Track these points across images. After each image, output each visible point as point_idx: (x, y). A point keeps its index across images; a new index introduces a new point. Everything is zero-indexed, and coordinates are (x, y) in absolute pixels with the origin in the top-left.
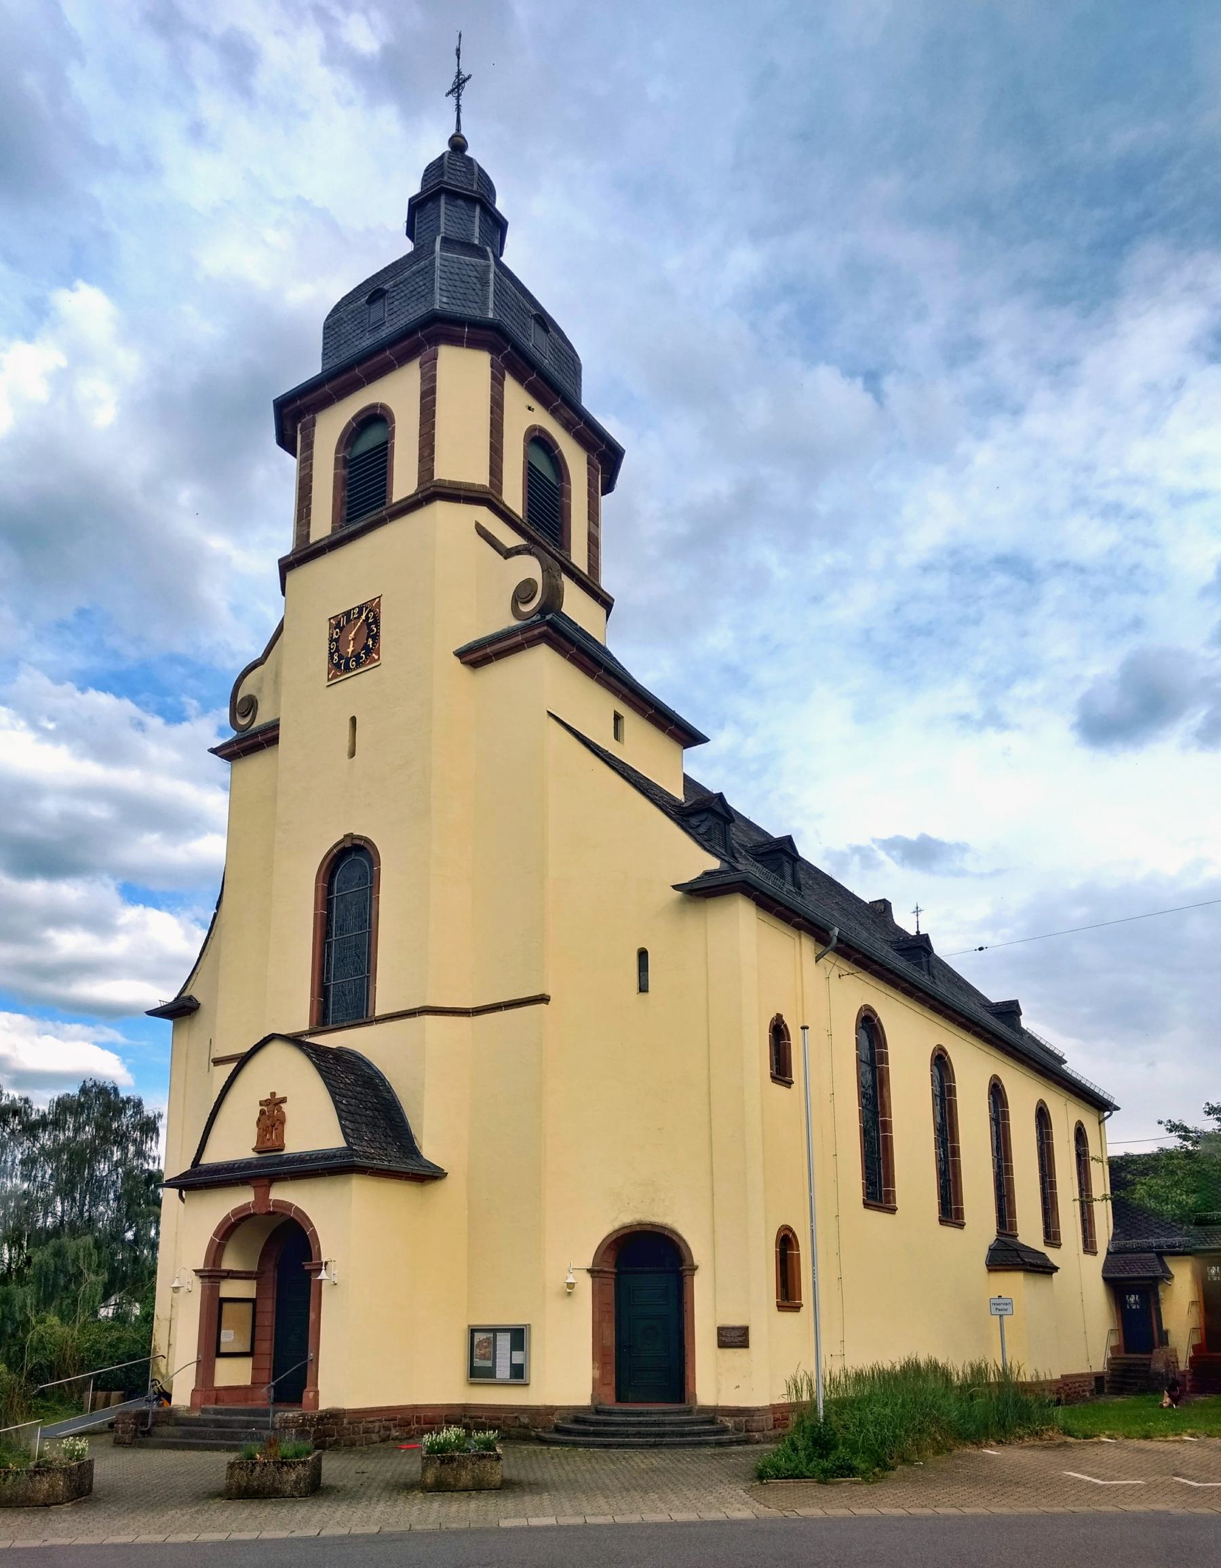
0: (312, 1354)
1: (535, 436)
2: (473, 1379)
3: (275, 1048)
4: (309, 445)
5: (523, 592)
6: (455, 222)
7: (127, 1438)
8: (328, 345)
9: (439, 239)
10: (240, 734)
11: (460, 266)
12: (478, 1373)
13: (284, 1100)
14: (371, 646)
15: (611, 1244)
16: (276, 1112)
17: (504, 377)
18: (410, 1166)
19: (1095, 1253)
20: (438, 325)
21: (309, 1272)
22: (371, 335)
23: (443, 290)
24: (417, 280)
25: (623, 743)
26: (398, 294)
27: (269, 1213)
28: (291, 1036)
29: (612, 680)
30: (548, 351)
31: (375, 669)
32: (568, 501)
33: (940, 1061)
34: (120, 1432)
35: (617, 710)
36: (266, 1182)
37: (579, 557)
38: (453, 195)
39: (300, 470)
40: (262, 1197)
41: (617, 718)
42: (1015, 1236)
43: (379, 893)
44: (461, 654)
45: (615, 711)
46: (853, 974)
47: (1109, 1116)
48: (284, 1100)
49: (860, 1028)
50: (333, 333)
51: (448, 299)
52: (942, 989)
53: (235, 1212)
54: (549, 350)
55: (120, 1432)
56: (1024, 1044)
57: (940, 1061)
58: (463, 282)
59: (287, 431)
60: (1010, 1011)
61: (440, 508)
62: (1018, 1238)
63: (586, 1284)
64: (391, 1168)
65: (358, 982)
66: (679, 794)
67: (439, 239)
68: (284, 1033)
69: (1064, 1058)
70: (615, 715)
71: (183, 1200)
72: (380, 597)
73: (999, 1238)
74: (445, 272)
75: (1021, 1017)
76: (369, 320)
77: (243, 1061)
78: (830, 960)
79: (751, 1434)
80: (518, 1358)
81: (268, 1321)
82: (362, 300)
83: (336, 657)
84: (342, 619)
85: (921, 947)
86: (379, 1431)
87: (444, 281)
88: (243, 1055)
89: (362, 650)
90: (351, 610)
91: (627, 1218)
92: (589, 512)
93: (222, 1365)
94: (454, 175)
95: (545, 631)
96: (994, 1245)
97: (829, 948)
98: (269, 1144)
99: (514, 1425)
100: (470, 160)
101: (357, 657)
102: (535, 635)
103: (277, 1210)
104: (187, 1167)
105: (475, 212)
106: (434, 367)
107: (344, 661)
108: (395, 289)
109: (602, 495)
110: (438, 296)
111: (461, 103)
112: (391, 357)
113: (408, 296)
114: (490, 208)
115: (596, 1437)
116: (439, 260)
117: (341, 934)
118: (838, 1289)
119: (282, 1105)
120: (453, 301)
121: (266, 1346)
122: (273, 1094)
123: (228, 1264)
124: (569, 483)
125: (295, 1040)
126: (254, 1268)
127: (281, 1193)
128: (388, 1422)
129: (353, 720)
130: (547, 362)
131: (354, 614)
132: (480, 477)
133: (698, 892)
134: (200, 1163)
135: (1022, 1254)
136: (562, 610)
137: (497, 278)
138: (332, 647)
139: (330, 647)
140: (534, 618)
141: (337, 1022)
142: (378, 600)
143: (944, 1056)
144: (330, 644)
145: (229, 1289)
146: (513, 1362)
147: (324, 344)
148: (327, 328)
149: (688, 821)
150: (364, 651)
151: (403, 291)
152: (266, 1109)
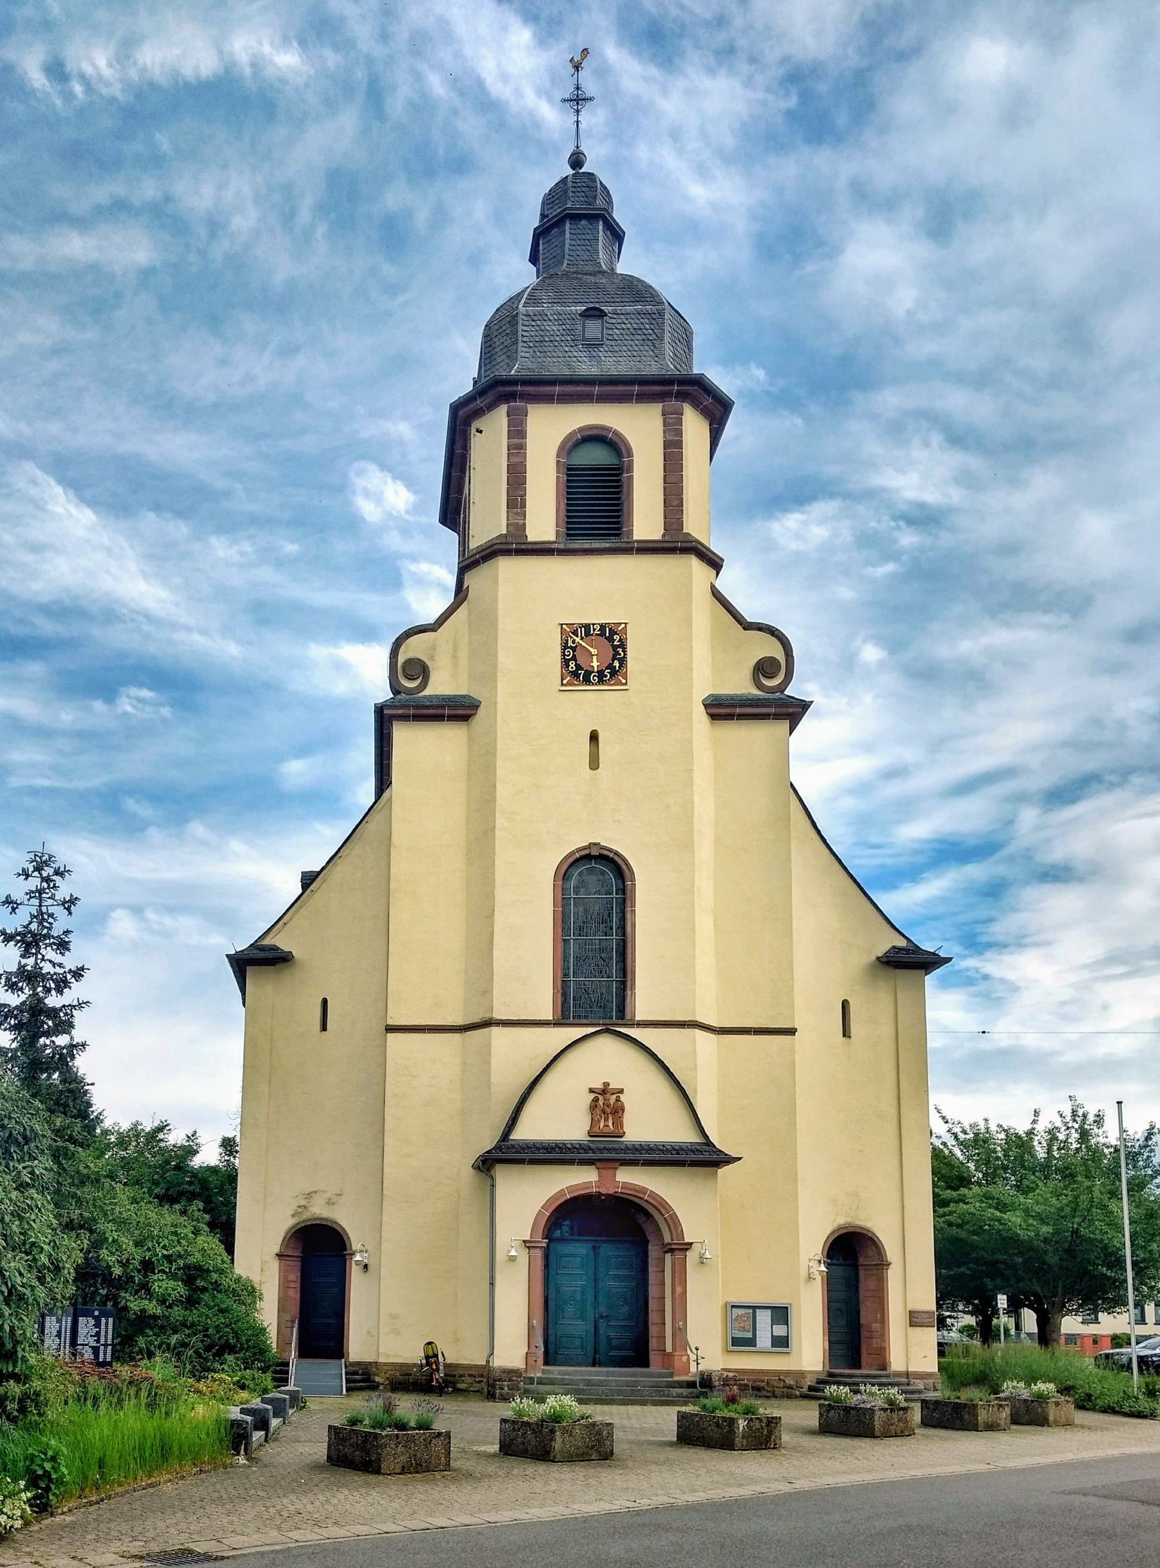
12: (742, 1343)
14: (617, 668)
20: (696, 388)
72: (626, 624)
80: (780, 1330)
89: (606, 669)
91: (842, 1221)
99: (779, 1385)
101: (601, 674)
134: (511, 1138)
141: (579, 1017)
146: (774, 1334)
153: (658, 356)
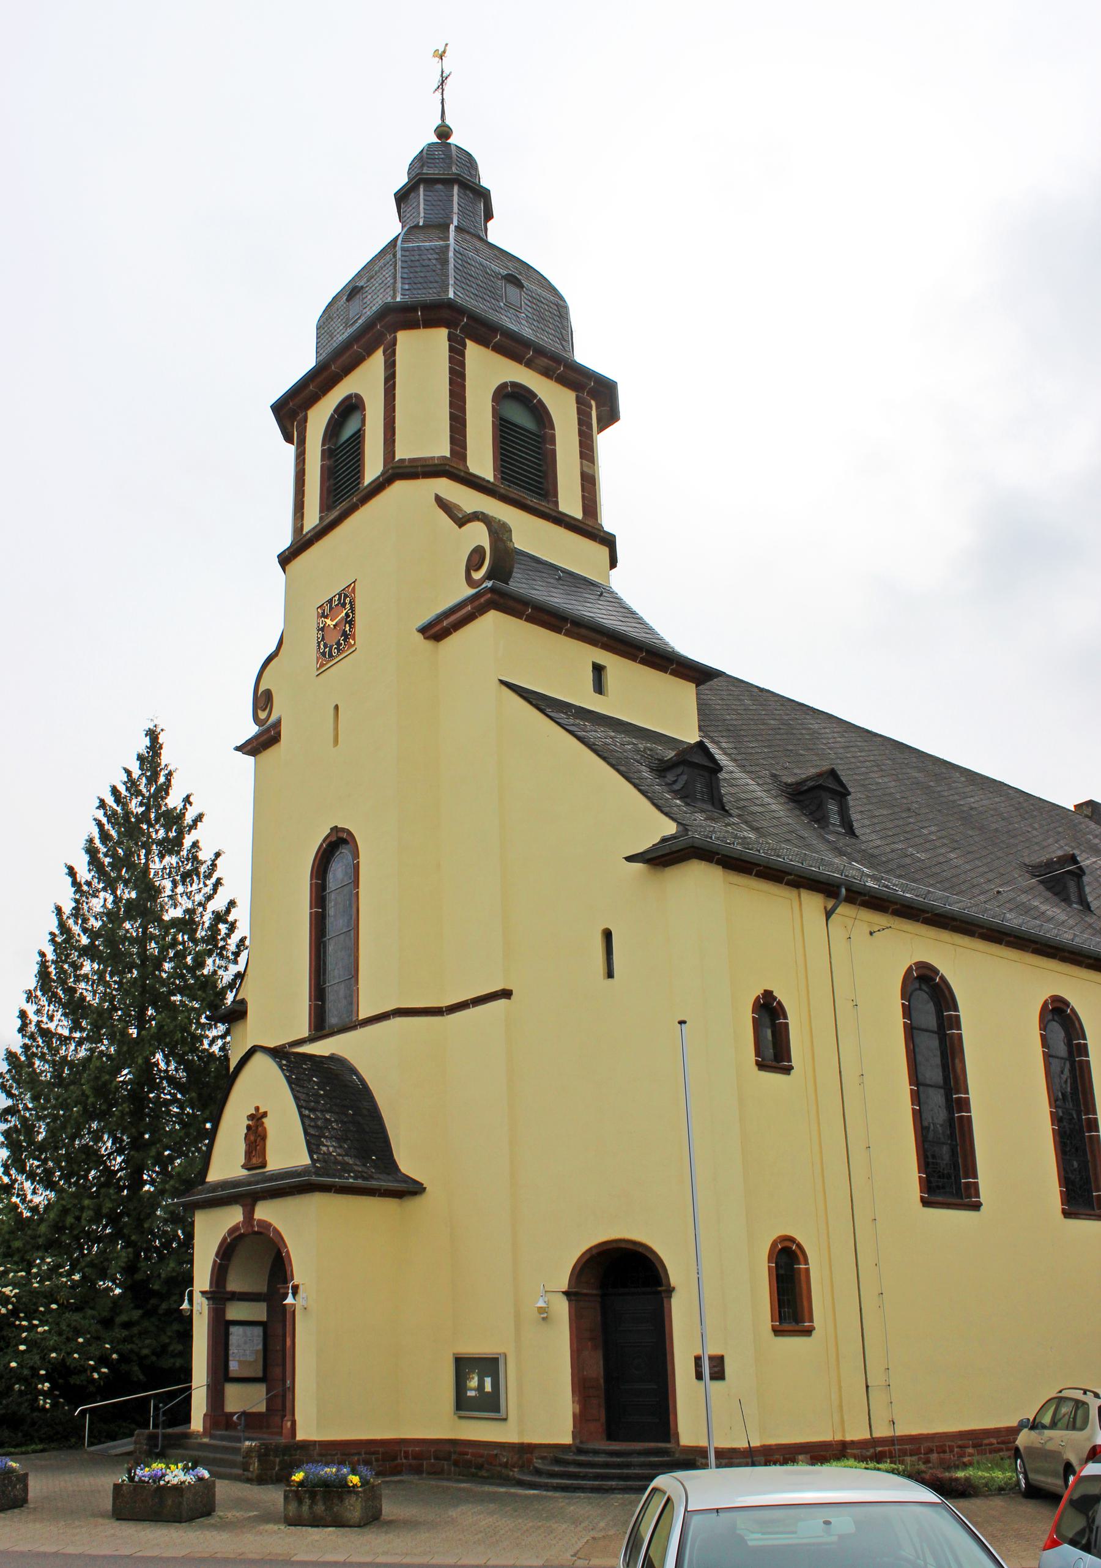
10: (261, 728)
11: (421, 252)
12: (463, 1404)
17: (464, 346)
23: (405, 278)
25: (608, 696)
29: (583, 631)
31: (352, 654)
35: (595, 661)
38: (430, 182)
40: (249, 1214)
44: (424, 630)
48: (265, 1114)
50: (323, 331)
58: (424, 266)
61: (399, 487)
63: (562, 1308)
72: (354, 582)
74: (406, 262)
83: (322, 646)
87: (406, 270)
102: (481, 604)
103: (261, 1230)
106: (394, 353)
115: (602, 1480)
120: (415, 286)
123: (233, 1285)
126: (264, 1289)
127: (264, 1212)
129: (336, 707)
132: (442, 449)
133: (657, 861)
145: (235, 1312)
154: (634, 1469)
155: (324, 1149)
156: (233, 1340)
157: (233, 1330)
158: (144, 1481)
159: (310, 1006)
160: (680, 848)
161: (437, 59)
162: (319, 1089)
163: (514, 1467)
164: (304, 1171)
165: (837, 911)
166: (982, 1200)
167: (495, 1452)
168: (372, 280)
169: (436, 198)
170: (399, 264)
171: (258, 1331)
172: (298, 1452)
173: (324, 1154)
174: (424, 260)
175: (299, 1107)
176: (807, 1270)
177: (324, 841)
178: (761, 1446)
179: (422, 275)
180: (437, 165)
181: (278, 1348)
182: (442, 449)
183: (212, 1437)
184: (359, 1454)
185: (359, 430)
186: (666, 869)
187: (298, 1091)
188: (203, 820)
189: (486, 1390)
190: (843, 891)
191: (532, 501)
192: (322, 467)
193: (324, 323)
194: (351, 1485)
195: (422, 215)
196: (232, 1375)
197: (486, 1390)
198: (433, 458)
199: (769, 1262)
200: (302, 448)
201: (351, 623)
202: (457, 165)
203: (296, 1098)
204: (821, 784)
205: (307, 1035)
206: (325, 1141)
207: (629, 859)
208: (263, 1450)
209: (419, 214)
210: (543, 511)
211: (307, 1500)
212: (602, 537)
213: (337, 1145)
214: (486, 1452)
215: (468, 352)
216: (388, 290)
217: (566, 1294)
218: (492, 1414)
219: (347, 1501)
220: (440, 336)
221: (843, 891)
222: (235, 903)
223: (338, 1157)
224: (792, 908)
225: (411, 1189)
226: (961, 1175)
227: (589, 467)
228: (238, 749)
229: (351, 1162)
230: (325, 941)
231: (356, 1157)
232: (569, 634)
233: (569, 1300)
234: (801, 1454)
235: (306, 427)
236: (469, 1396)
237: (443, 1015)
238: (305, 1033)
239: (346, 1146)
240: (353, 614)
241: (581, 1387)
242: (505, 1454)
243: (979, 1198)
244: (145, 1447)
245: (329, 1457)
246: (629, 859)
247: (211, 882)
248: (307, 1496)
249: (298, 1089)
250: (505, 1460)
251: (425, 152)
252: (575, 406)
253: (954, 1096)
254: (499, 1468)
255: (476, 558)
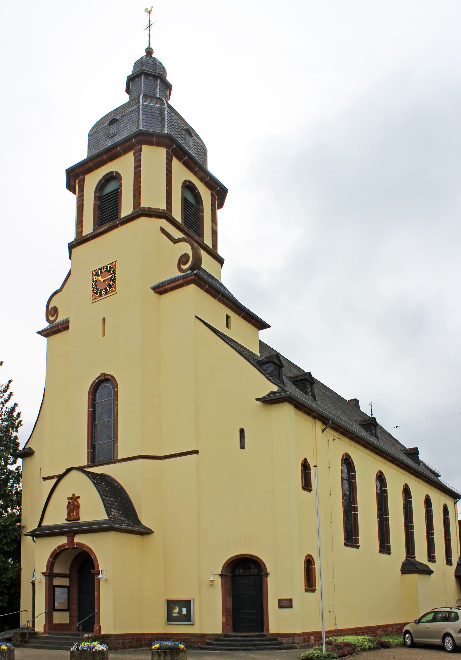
0: (97, 610)
1: (187, 185)
2: (168, 622)
3: (74, 473)
4: (82, 190)
5: (183, 259)
6: (148, 87)
7: (18, 643)
8: (91, 144)
9: (141, 96)
10: (50, 325)
12: (170, 618)
13: (79, 497)
14: (112, 284)
15: (230, 563)
16: (75, 503)
17: (172, 158)
18: (136, 528)
19: (451, 565)
21: (94, 575)
22: (110, 140)
24: (132, 115)
25: (230, 329)
26: (123, 121)
27: (74, 548)
28: (79, 468)
29: (225, 300)
30: (192, 145)
32: (202, 214)
33: (380, 477)
34: (15, 640)
36: (72, 534)
37: (208, 241)
38: (147, 75)
39: (78, 201)
40: (71, 541)
41: (228, 317)
42: (414, 558)
43: (117, 401)
45: (226, 314)
46: (339, 439)
47: (458, 501)
48: (79, 497)
49: (343, 463)
50: (93, 138)
51: (146, 124)
52: (380, 444)
53: (59, 547)
54: (193, 145)
55: (15, 640)
56: (420, 469)
57: (380, 477)
58: (153, 116)
59: (71, 183)
60: (414, 453)
61: (143, 220)
62: (416, 559)
63: (219, 581)
64: (129, 529)
65: (109, 443)
66: (256, 351)
67: (141, 96)
68: (76, 466)
69: (439, 474)
70: (226, 315)
71: (35, 542)
72: (116, 261)
73: (407, 559)
74: (144, 111)
75: (419, 455)
76: (110, 132)
77: (60, 478)
78: (329, 430)
79: (293, 645)
81: (75, 595)
82: (106, 124)
83: (95, 290)
84: (98, 272)
85: (372, 424)
86: (128, 644)
87: (144, 116)
88: (60, 476)
89: (108, 286)
90: (102, 267)
92: (212, 219)
93: (56, 614)
94: (148, 66)
95: (194, 278)
96: (405, 562)
97: (328, 426)
98: (73, 517)
100: (155, 59)
103: (78, 547)
104: (36, 527)
105: (157, 82)
106: (140, 155)
107: (99, 291)
108: (122, 118)
109: (218, 209)
110: (142, 122)
111: (150, 34)
112: (120, 150)
113: (128, 122)
114: (165, 80)
116: (142, 106)
117: (100, 420)
118: (333, 582)
119: (78, 500)
121: (75, 607)
122: (74, 495)
123: (56, 570)
124: (202, 205)
125: (81, 469)
126: (68, 573)
127: (78, 539)
128: (132, 640)
129: (104, 319)
130: (192, 151)
131: (104, 269)
132: (163, 206)
133: (268, 402)
135: (416, 565)
136: (201, 267)
137: (169, 114)
138: (94, 285)
139: (93, 285)
140: (188, 272)
142: (115, 263)
143: (382, 475)
144: (93, 283)
145: (57, 581)
147: (89, 143)
148: (90, 136)
149: (262, 367)
150: (109, 287)
151: (125, 120)
152: (70, 501)
153: (163, 128)
154: (256, 642)
155: (113, 513)
156: (56, 593)
157: (57, 589)
158: (85, 650)
159: (88, 452)
160: (282, 397)
161: (147, 13)
162: (106, 488)
163: (198, 643)
164: (105, 522)
165: (326, 430)
166: (360, 544)
167: (188, 637)
168: (124, 117)
169: (149, 84)
170: (141, 112)
171: (66, 590)
172: (107, 638)
173: (113, 515)
174: (153, 113)
175: (101, 495)
176: (315, 567)
177: (97, 379)
178: (302, 632)
179: (152, 120)
180: (150, 67)
181: (74, 597)
182: (163, 206)
183: (49, 634)
184: (128, 639)
185: (118, 189)
186: (272, 405)
187: (99, 488)
188: (2, 365)
189: (183, 613)
190: (331, 421)
191: (196, 237)
192: (94, 204)
193: (93, 134)
194: (181, 648)
195: (143, 90)
196: (56, 608)
197: (183, 613)
198: (159, 209)
199: (304, 564)
200: (82, 193)
201: (114, 280)
202: (159, 70)
203: (99, 491)
204: (306, 378)
205: (87, 465)
206: (112, 510)
207: (257, 400)
208: (94, 638)
209: (141, 89)
210: (200, 243)
211: (163, 655)
212: (220, 259)
213: (117, 512)
214: (183, 638)
215: (173, 162)
216: (134, 124)
217: (220, 575)
218: (188, 622)
219: (180, 655)
220: (163, 151)
221: (331, 421)
222: (17, 404)
223: (118, 517)
224: (313, 426)
225: (147, 532)
226: (353, 535)
227: (215, 227)
228: (39, 333)
229: (124, 520)
230: (96, 424)
231: (124, 517)
232: (219, 300)
233: (222, 578)
234: (311, 636)
235: (84, 183)
236: (173, 616)
237: (161, 460)
238: (85, 463)
239: (120, 512)
240: (115, 276)
241: (225, 611)
242: (193, 638)
243: (359, 544)
244: (20, 638)
245: (118, 640)
246: (257, 400)
247: (6, 394)
248: (163, 653)
249: (99, 487)
250: (193, 640)
251: (144, 59)
252: (210, 197)
253: (352, 505)
254: (190, 644)
255: (184, 259)
